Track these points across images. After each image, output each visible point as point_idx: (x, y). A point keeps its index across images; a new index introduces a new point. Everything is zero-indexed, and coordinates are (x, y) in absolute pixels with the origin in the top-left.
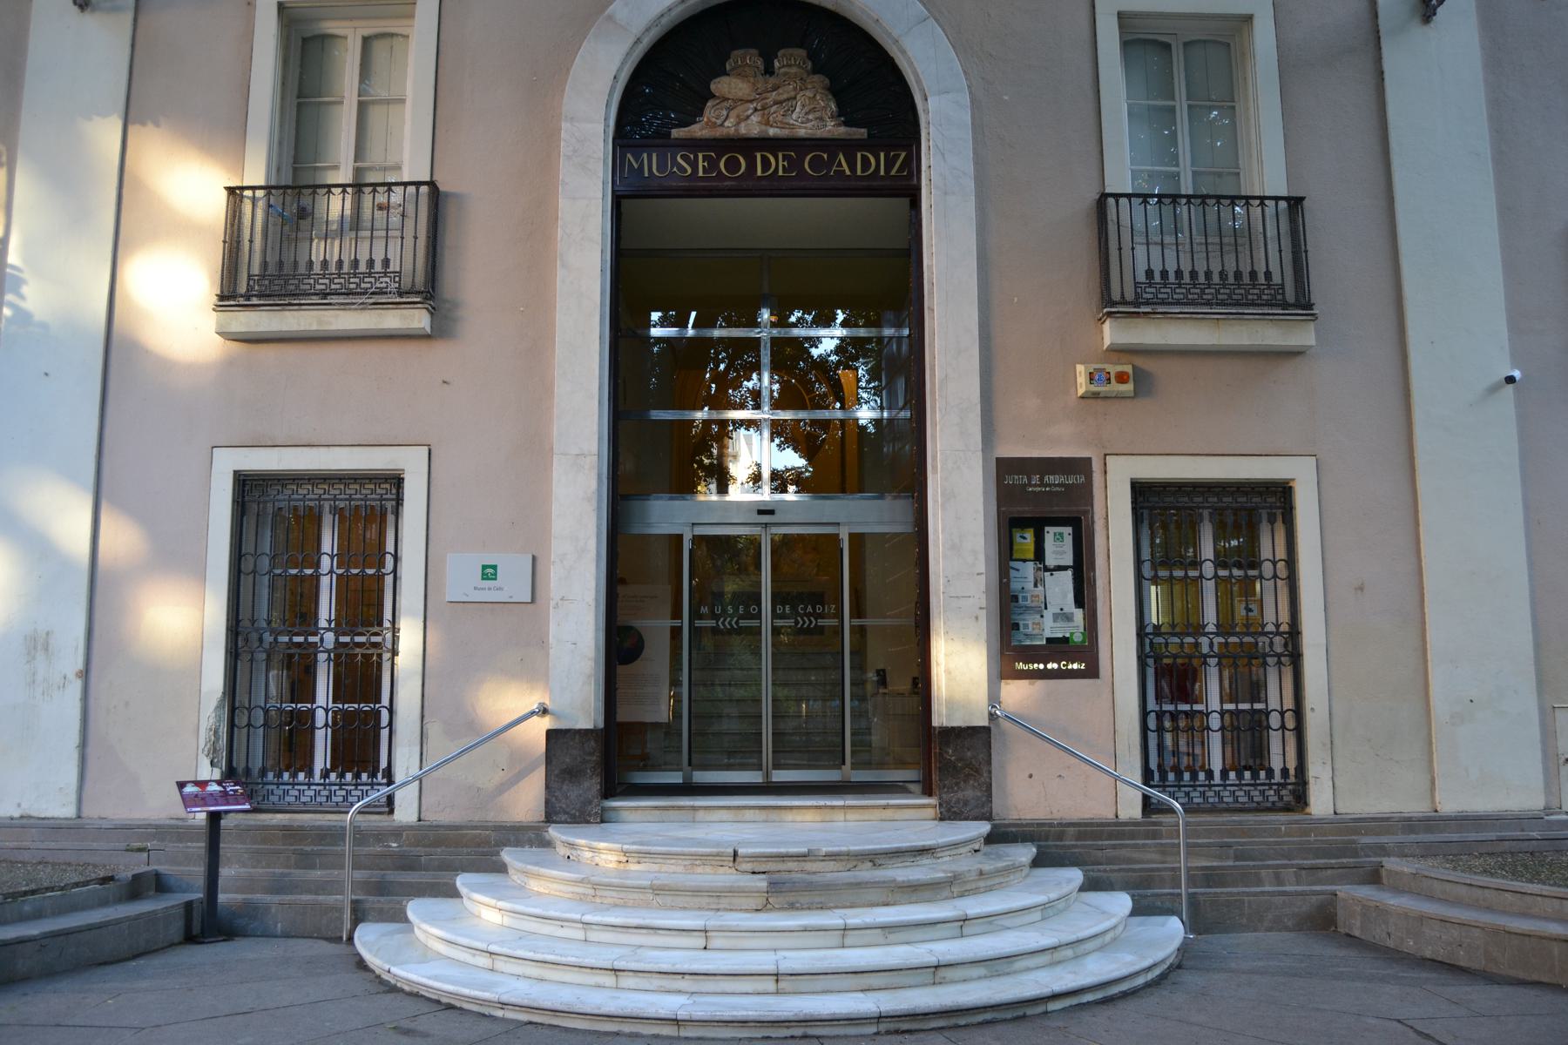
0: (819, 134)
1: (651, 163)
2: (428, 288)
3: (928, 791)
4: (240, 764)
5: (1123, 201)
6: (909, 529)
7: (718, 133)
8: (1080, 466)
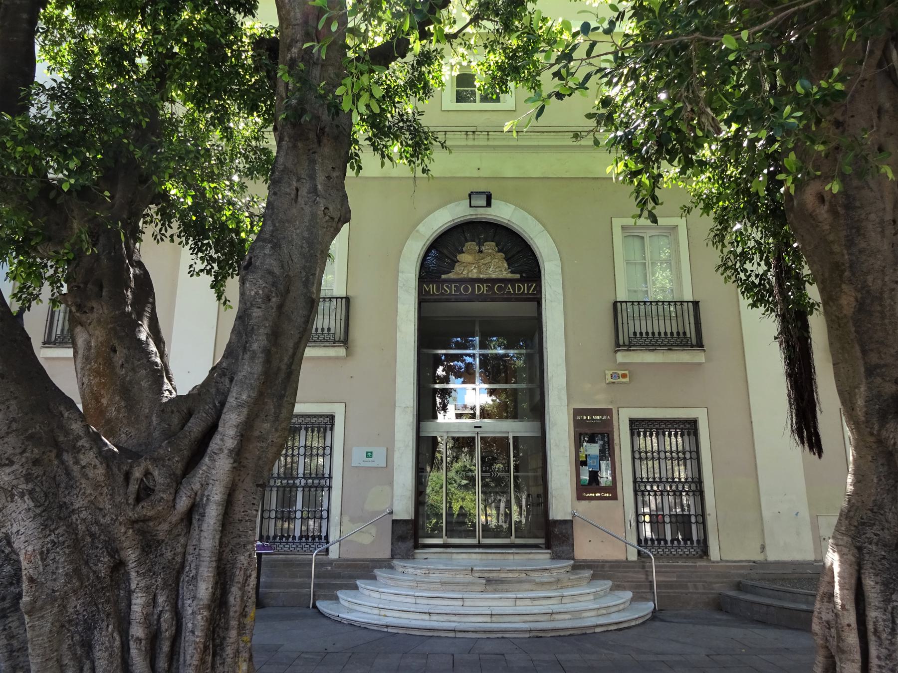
0: (501, 277)
1: (432, 288)
2: (345, 341)
3: (548, 546)
4: (265, 534)
5: (624, 304)
6: (537, 434)
7: (461, 276)
8: (607, 412)
